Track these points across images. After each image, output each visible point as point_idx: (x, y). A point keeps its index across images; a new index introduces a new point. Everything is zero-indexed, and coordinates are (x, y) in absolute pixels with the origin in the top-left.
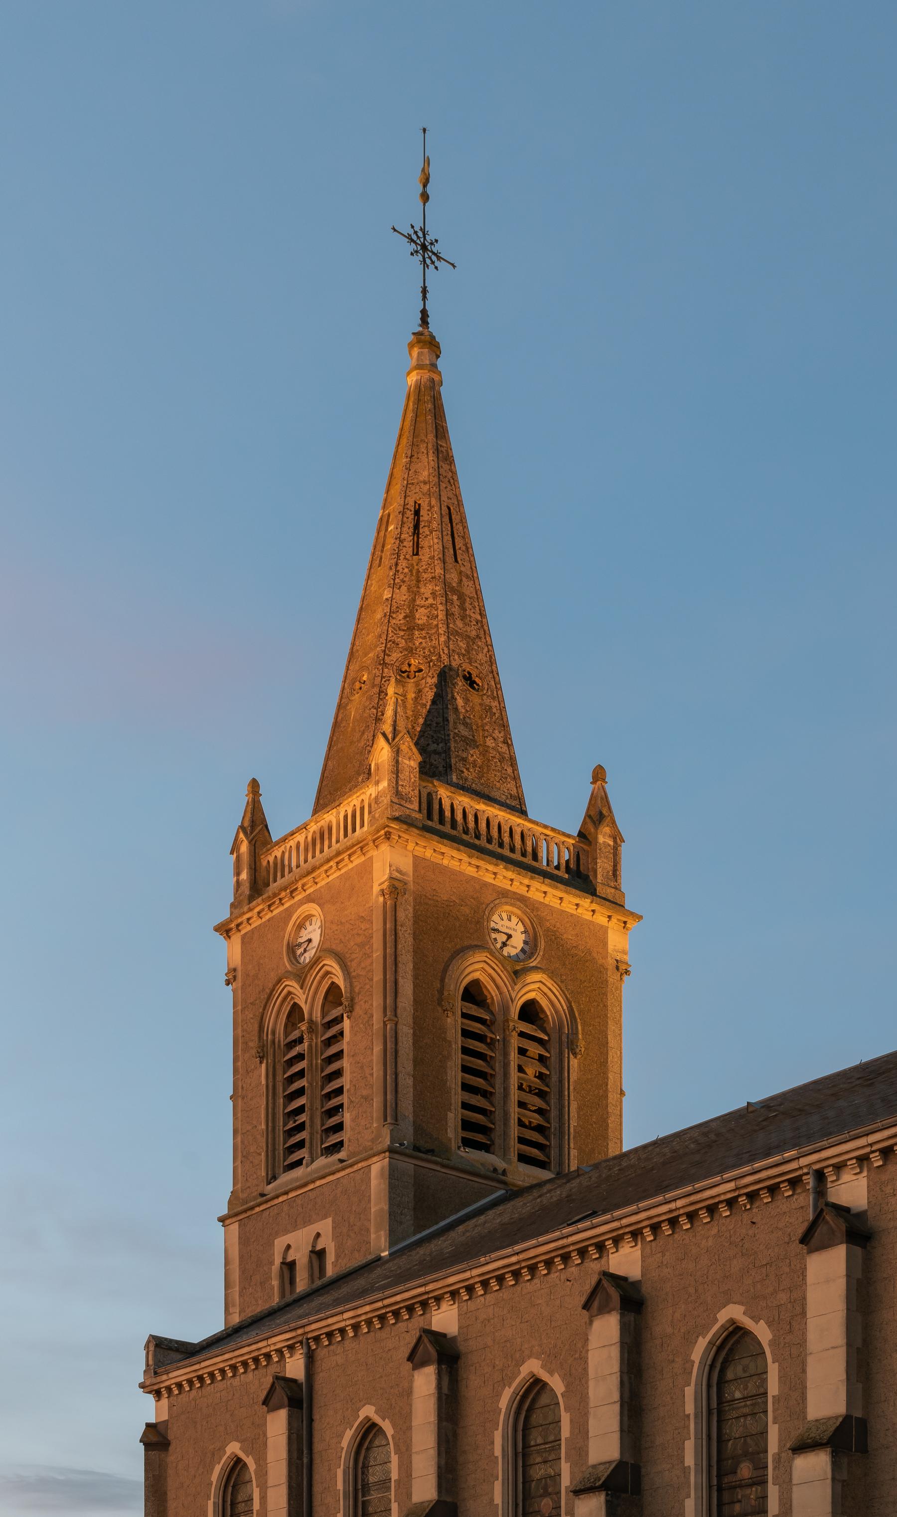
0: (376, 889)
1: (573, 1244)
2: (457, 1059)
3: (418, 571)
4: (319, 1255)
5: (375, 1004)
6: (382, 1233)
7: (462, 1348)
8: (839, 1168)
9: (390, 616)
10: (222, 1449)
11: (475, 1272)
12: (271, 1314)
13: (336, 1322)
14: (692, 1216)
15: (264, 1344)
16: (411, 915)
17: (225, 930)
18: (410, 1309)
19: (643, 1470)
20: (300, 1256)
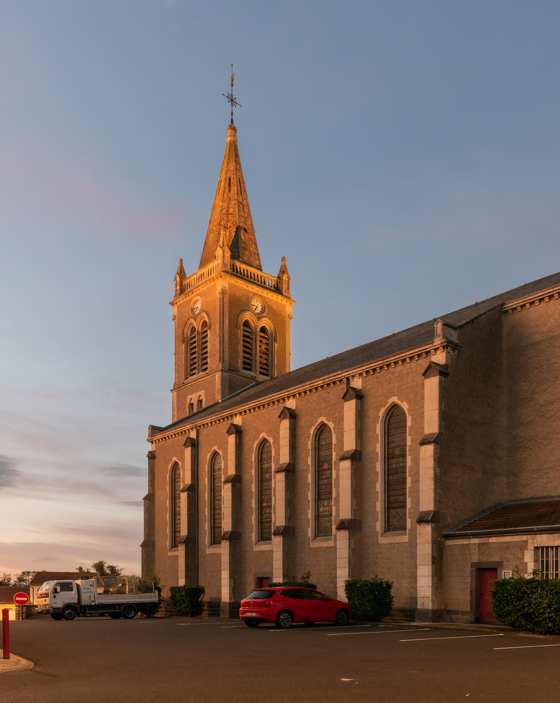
0: (217, 292)
4: (200, 401)
8: (353, 377)
10: (171, 459)
11: (247, 407)
12: (186, 419)
14: (310, 391)
20: (195, 402)
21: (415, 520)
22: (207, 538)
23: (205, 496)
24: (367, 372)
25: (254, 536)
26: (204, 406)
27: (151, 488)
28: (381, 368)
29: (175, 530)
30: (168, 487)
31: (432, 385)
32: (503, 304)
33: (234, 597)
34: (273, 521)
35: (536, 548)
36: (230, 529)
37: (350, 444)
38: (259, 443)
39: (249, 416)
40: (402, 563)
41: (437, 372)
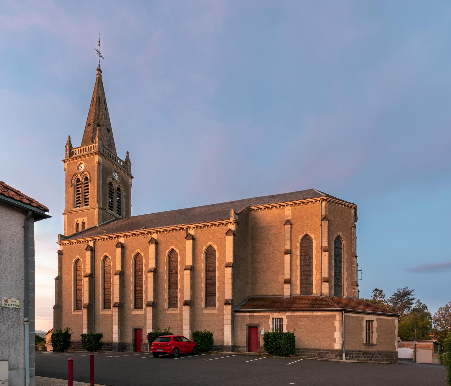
0: (96, 162)
2: (108, 195)
4: (84, 223)
7: (125, 245)
8: (190, 228)
9: (95, 115)
10: (75, 256)
12: (74, 235)
13: (100, 237)
14: (166, 231)
18: (115, 238)
22: (100, 305)
23: (99, 281)
24: (197, 227)
25: (132, 306)
26: (86, 228)
28: (204, 226)
30: (72, 273)
31: (230, 239)
32: (250, 207)
34: (82, 300)
35: (273, 318)
36: (119, 301)
37: (189, 262)
39: (128, 238)
40: (214, 323)
41: (232, 234)
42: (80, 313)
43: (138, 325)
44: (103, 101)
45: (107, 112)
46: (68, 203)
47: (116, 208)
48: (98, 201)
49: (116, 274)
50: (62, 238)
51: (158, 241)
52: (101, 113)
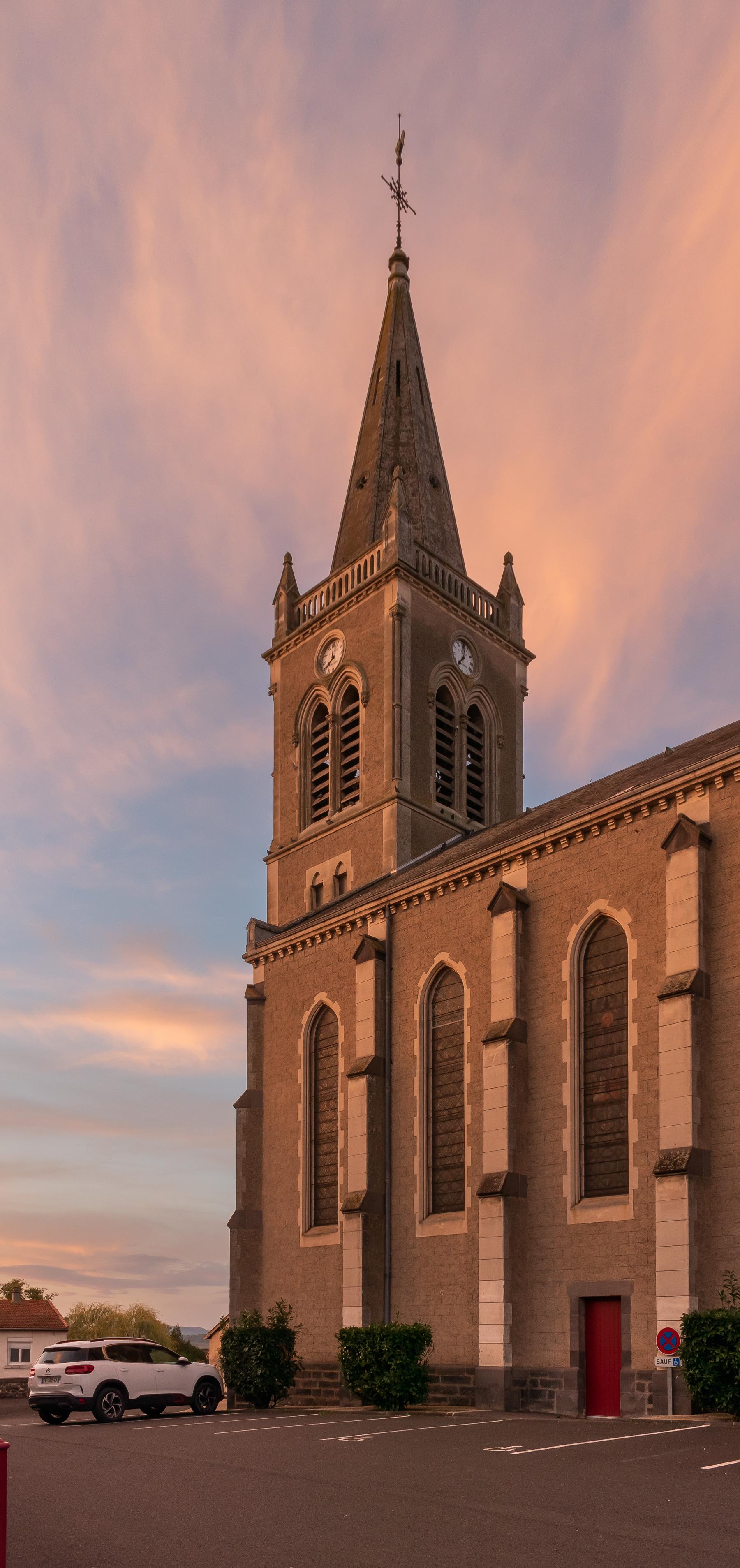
0: (387, 612)
1: (644, 799)
2: (433, 741)
3: (400, 408)
4: (340, 878)
5: (385, 694)
6: (392, 857)
7: (531, 897)
9: (383, 436)
10: (312, 999)
11: (548, 834)
12: (306, 919)
13: (415, 889)
15: (352, 913)
16: (409, 632)
17: (269, 656)
19: (712, 979)
20: (326, 880)
21: (651, 1169)
22: (417, 1198)
25: (569, 1184)
27: (253, 1077)
29: (321, 1185)
30: (301, 1072)
33: (515, 1353)
38: (582, 929)
39: (552, 859)
42: (331, 1239)
43: (605, 1278)
44: (412, 371)
45: (430, 414)
46: (283, 814)
47: (465, 795)
48: (397, 772)
49: (492, 1039)
50: (261, 931)
51: (713, 830)
52: (406, 420)
